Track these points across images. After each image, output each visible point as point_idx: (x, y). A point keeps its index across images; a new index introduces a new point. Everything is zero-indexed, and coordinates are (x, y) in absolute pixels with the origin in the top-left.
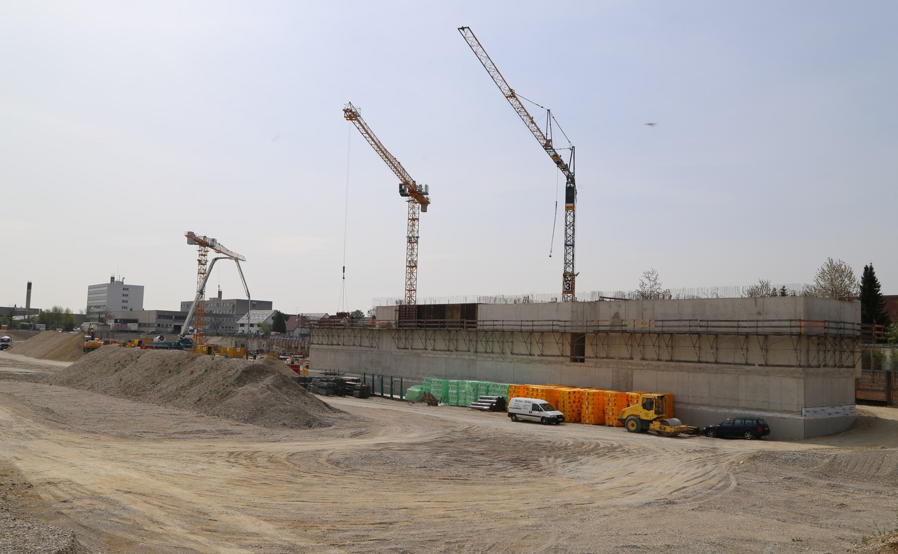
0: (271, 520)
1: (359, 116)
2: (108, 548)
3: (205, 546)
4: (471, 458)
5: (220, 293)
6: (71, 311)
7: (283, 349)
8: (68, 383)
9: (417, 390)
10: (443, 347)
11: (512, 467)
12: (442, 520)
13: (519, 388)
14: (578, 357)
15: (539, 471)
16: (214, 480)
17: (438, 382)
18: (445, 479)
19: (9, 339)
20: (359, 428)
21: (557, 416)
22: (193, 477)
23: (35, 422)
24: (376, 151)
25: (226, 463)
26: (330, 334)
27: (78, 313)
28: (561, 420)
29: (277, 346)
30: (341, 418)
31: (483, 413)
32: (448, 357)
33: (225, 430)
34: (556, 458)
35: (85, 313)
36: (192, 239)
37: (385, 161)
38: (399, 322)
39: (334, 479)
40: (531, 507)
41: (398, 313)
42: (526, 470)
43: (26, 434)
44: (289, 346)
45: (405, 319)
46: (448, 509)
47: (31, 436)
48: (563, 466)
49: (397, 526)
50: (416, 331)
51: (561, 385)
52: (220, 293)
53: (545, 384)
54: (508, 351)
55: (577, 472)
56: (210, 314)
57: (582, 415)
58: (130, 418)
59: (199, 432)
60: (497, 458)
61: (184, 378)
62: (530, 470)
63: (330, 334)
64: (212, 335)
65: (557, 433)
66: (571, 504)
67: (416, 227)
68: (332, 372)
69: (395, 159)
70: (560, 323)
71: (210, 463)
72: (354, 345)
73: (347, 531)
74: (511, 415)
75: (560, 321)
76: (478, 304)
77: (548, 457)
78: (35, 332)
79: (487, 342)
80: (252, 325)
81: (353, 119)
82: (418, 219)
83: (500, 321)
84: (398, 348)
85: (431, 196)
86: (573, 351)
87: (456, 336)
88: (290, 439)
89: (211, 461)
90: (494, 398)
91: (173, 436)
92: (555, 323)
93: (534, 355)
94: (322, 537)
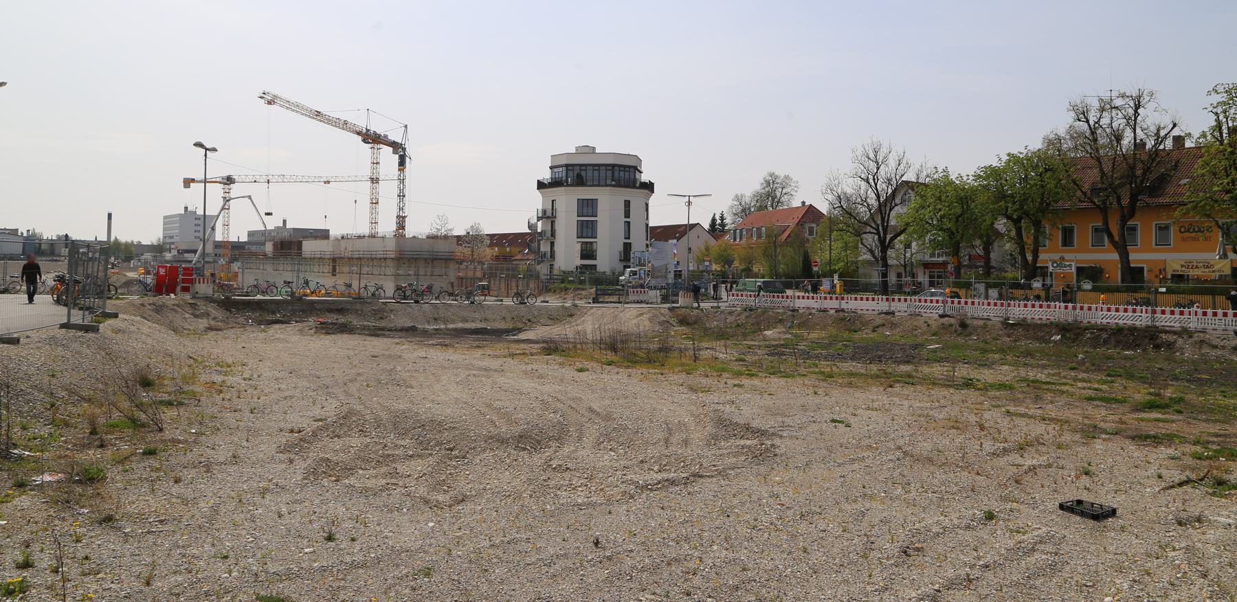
5: (285, 222)
52: (285, 222)
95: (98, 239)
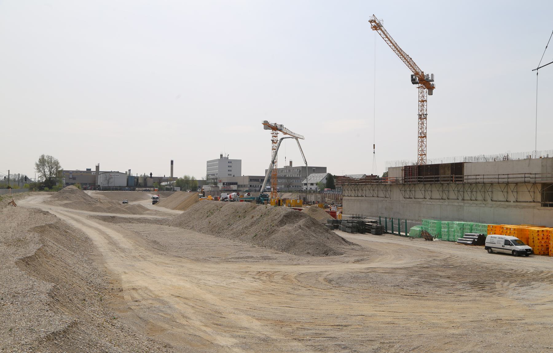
0: (261, 319)
1: (382, 26)
2: (148, 333)
3: (209, 334)
4: (438, 280)
5: (291, 162)
6: (195, 178)
7: (333, 200)
8: (180, 224)
9: (418, 229)
10: (438, 197)
11: (469, 288)
12: (387, 325)
13: (496, 227)
14: (548, 203)
15: (491, 292)
16: (237, 290)
17: (433, 223)
18: (406, 295)
19: (157, 197)
20: (362, 256)
21: (526, 249)
22: (225, 288)
23: (146, 250)
24: (394, 50)
25: (252, 279)
26: (356, 189)
27: (201, 179)
28: (530, 252)
29: (328, 198)
30: (353, 249)
31: (466, 247)
32: (404, 202)
33: (267, 257)
34: (511, 282)
35: (205, 179)
36: (267, 125)
37: (400, 58)
38: (405, 178)
39: (321, 292)
40: (465, 320)
41: (404, 172)
42: (480, 291)
43: (139, 258)
44: (337, 198)
45: (409, 176)
46: (396, 318)
47: (141, 259)
48: (515, 289)
49: (349, 328)
50: (434, 185)
51: (533, 225)
52: (291, 162)
53: (520, 224)
54: (489, 199)
55: (524, 294)
56: (285, 177)
57: (550, 249)
58: (207, 247)
59: (248, 257)
60: (459, 281)
61: (248, 220)
62: (484, 291)
63: (356, 189)
64: (286, 192)
65: (522, 263)
66: (501, 319)
67: (425, 107)
68: (357, 216)
69: (408, 55)
70: (531, 176)
71: (241, 279)
72: (373, 196)
73: (310, 330)
74: (487, 248)
75: (531, 174)
76: (464, 162)
77: (504, 281)
78: (174, 192)
79: (472, 192)
80: (312, 184)
81: (378, 28)
82: (426, 101)
83: (481, 175)
84: (404, 198)
85: (436, 83)
86: (543, 199)
87: (447, 188)
88: (308, 263)
89: (242, 277)
90: (476, 235)
91: (230, 260)
92: (526, 175)
93: (510, 202)
94: (288, 333)
95: (165, 176)
